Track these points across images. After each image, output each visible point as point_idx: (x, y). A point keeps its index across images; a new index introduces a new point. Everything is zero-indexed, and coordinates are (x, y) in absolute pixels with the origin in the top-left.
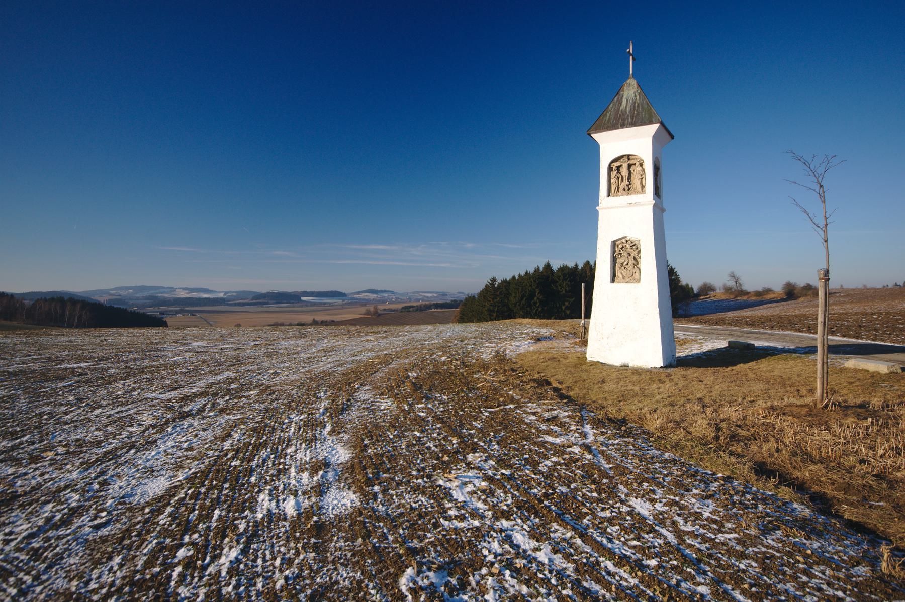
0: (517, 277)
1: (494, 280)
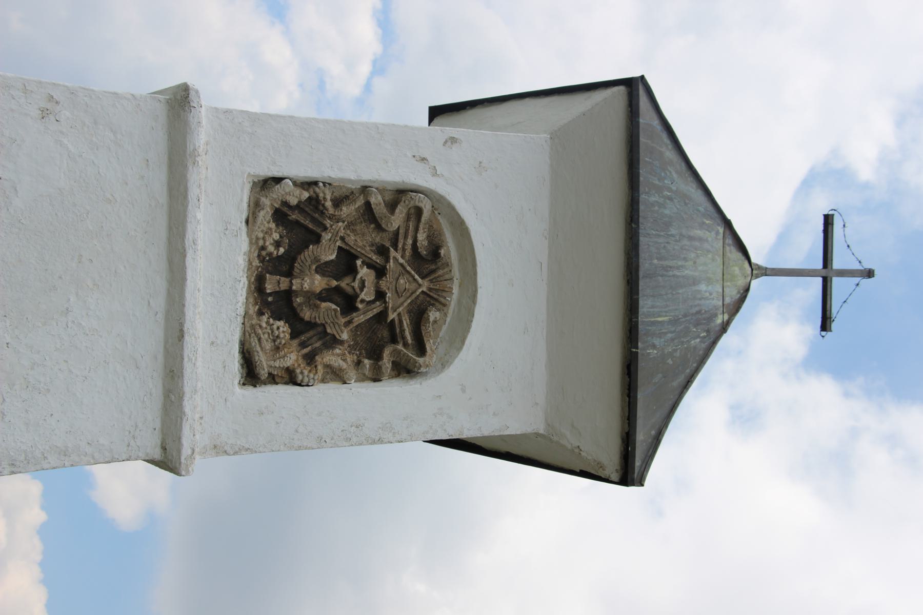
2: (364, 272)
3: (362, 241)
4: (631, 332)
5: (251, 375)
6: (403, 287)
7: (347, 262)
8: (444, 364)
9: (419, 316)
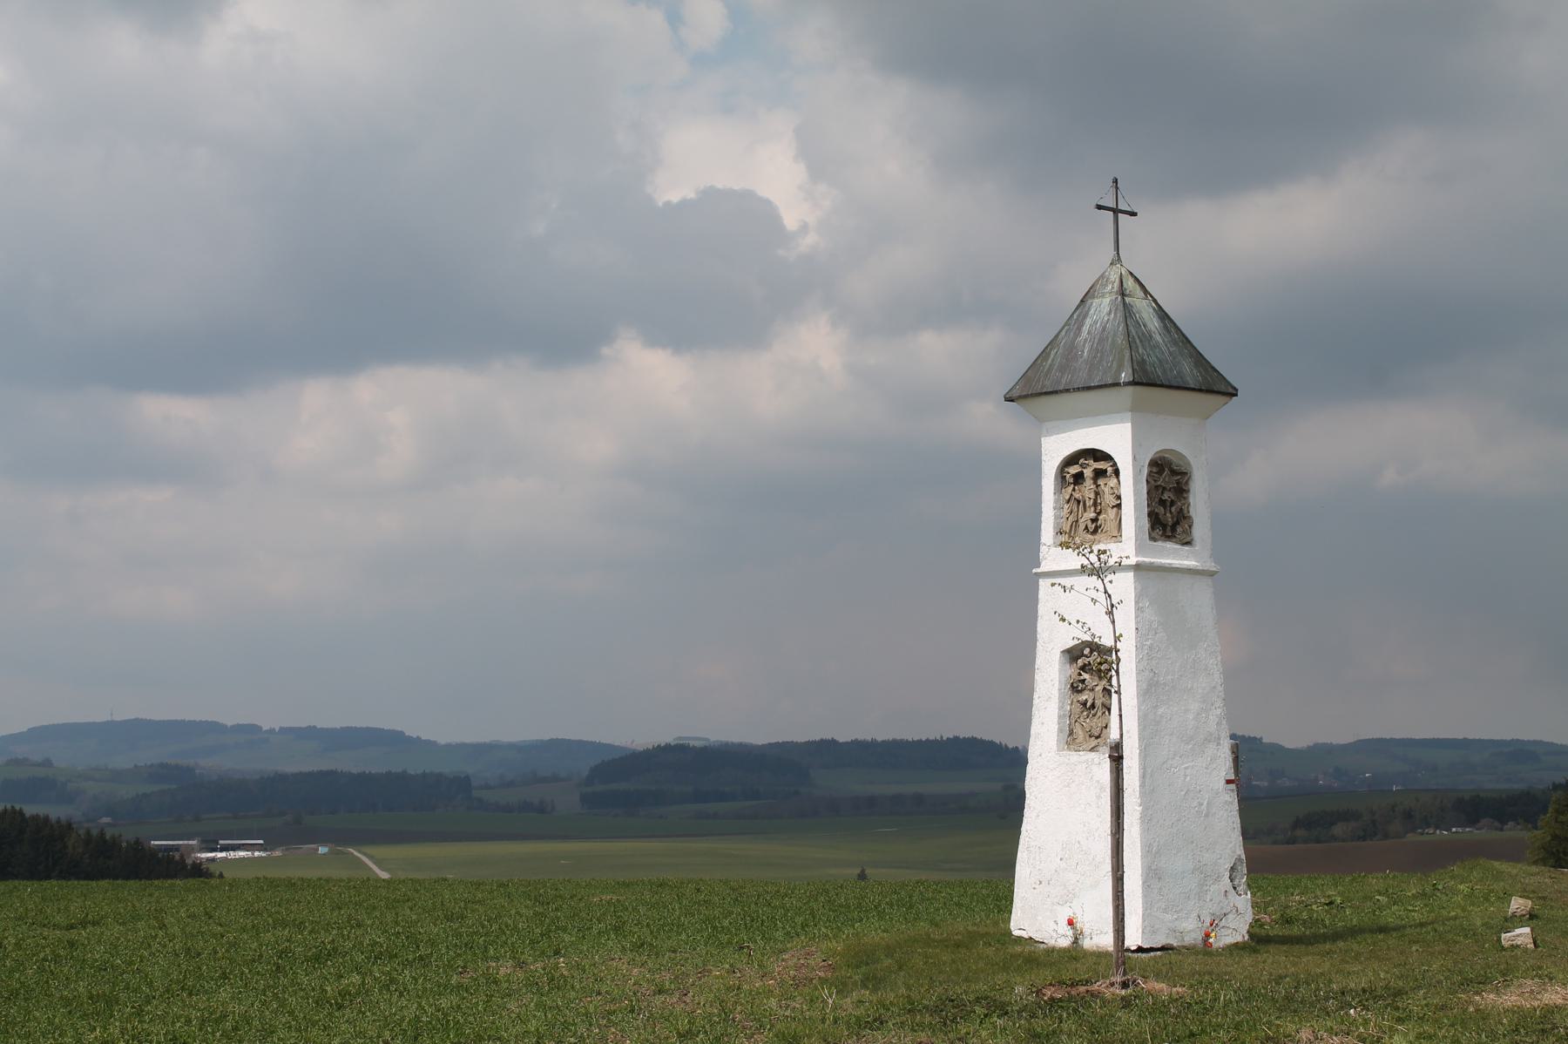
2: (1165, 497)
4: (1200, 390)
5: (1188, 543)
6: (1165, 479)
7: (1162, 502)
8: (1189, 464)
9: (1174, 472)
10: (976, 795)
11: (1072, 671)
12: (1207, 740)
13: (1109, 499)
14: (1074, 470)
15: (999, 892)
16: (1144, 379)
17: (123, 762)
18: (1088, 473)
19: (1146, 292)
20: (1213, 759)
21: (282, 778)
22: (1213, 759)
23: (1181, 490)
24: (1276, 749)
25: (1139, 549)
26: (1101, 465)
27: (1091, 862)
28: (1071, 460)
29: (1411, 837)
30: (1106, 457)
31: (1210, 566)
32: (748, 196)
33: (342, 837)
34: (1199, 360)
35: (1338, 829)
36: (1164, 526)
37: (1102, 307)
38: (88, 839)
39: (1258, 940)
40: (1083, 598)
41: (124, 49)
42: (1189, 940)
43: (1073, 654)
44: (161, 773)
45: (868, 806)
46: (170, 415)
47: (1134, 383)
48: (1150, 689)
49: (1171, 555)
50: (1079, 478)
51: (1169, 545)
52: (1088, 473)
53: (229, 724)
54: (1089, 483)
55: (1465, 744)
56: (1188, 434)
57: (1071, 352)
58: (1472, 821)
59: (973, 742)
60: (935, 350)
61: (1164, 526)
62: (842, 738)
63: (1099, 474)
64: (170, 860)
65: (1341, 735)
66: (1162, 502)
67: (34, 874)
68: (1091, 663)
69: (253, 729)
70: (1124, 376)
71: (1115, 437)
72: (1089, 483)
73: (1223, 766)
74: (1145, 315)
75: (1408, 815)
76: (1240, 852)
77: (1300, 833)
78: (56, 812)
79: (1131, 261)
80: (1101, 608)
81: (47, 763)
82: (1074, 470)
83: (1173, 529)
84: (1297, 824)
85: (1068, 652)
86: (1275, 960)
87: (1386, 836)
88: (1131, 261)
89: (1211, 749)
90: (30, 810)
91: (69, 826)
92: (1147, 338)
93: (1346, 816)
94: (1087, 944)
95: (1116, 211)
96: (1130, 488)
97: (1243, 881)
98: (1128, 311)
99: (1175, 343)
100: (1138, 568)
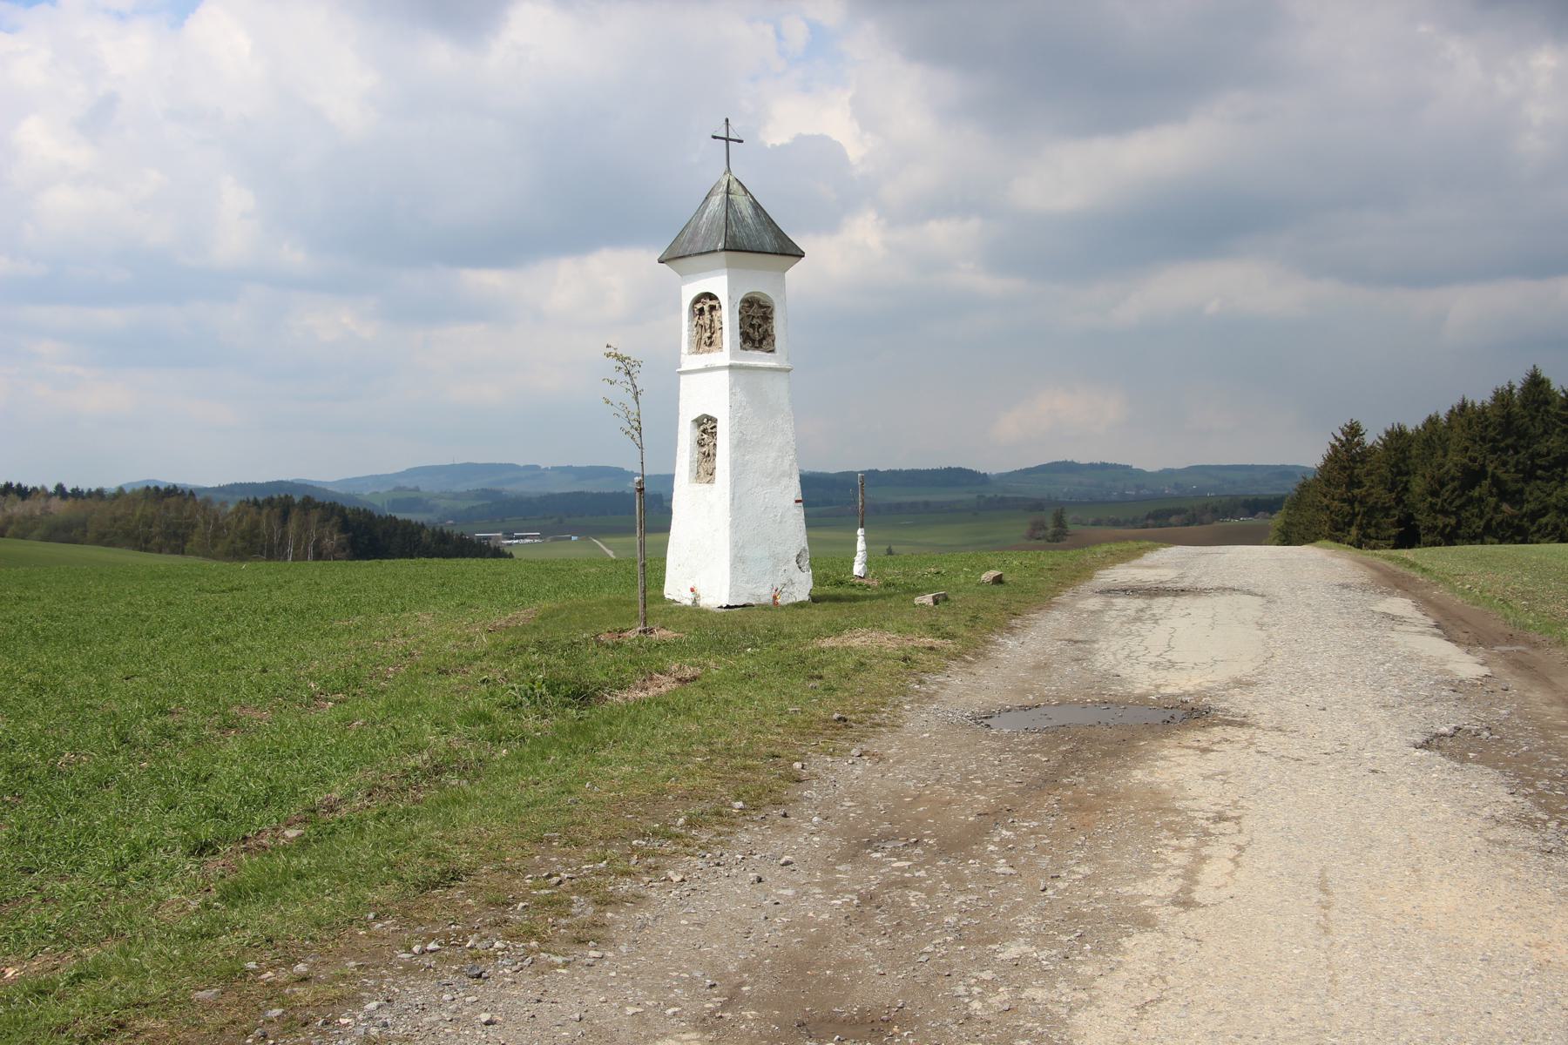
0: (1443, 416)
1: (1354, 431)
3: (748, 321)
6: (755, 311)
7: (752, 326)
9: (761, 307)
10: (646, 510)
11: (697, 433)
12: (783, 475)
13: (717, 325)
14: (699, 306)
15: (654, 570)
16: (733, 247)
17: (461, 488)
18: (706, 308)
19: (746, 191)
20: (786, 487)
21: (552, 496)
22: (786, 487)
23: (767, 317)
24: (1140, 473)
25: (732, 356)
26: (713, 303)
27: (715, 552)
28: (697, 300)
29: (1216, 524)
30: (716, 298)
31: (786, 365)
32: (823, 138)
33: (587, 532)
34: (780, 235)
35: (1173, 519)
36: (753, 341)
37: (717, 201)
38: (434, 533)
39: (815, 599)
40: (707, 384)
41: (439, 56)
42: (763, 600)
43: (699, 422)
44: (484, 493)
45: (898, 508)
46: (491, 280)
47: (725, 250)
48: (739, 445)
49: (757, 358)
50: (701, 310)
51: (757, 353)
52: (706, 308)
53: (522, 464)
54: (707, 315)
55: (1252, 467)
56: (758, 281)
57: (695, 233)
58: (1253, 514)
59: (960, 470)
60: (941, 233)
61: (753, 341)
62: (544, 463)
63: (712, 308)
64: (481, 545)
65: (1179, 464)
66: (752, 326)
67: (403, 554)
68: (706, 425)
69: (536, 467)
70: (720, 246)
71: (718, 283)
72: (707, 315)
73: (795, 491)
74: (742, 207)
75: (1215, 511)
76: (805, 545)
77: (1150, 522)
78: (416, 517)
79: (736, 172)
80: (631, 395)
81: (417, 489)
82: (699, 306)
83: (761, 342)
84: (1148, 517)
85: (696, 420)
86: (820, 615)
87: (1201, 523)
88: (736, 172)
89: (785, 481)
90: (400, 516)
91: (423, 526)
92: (740, 221)
93: (1178, 512)
94: (703, 603)
95: (727, 140)
96: (728, 320)
97: (806, 563)
98: (729, 203)
99: (762, 223)
100: (731, 367)
